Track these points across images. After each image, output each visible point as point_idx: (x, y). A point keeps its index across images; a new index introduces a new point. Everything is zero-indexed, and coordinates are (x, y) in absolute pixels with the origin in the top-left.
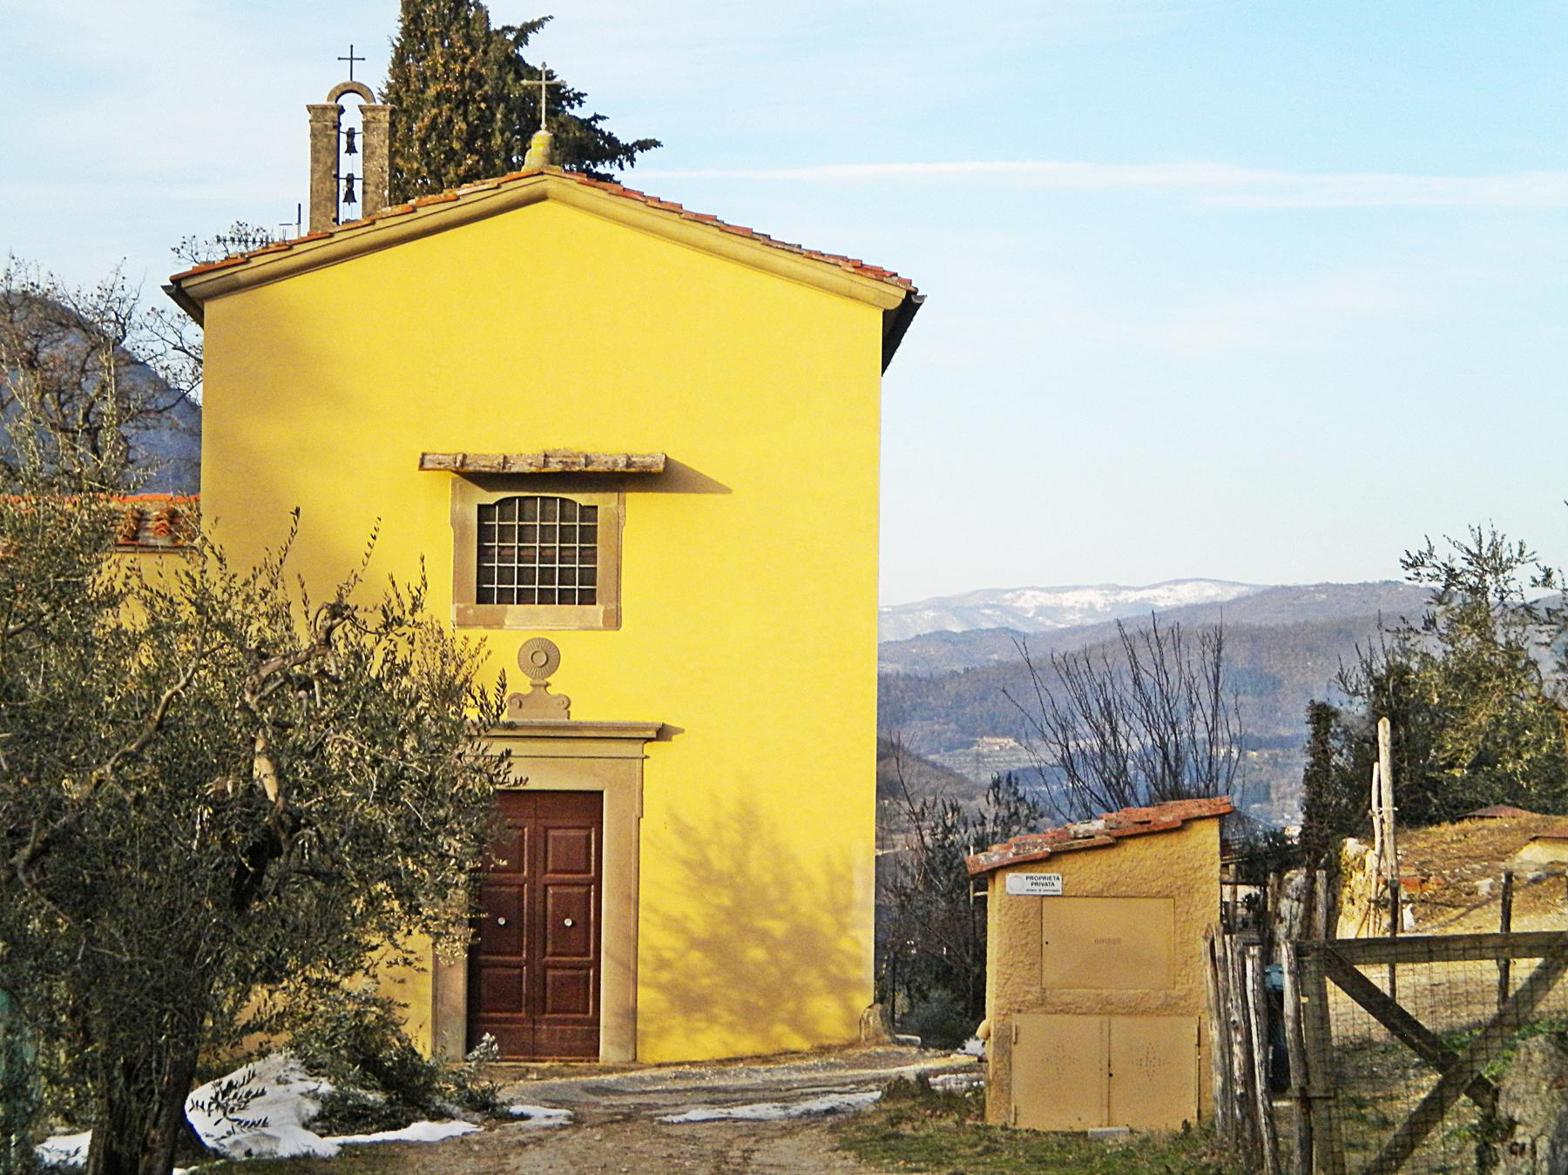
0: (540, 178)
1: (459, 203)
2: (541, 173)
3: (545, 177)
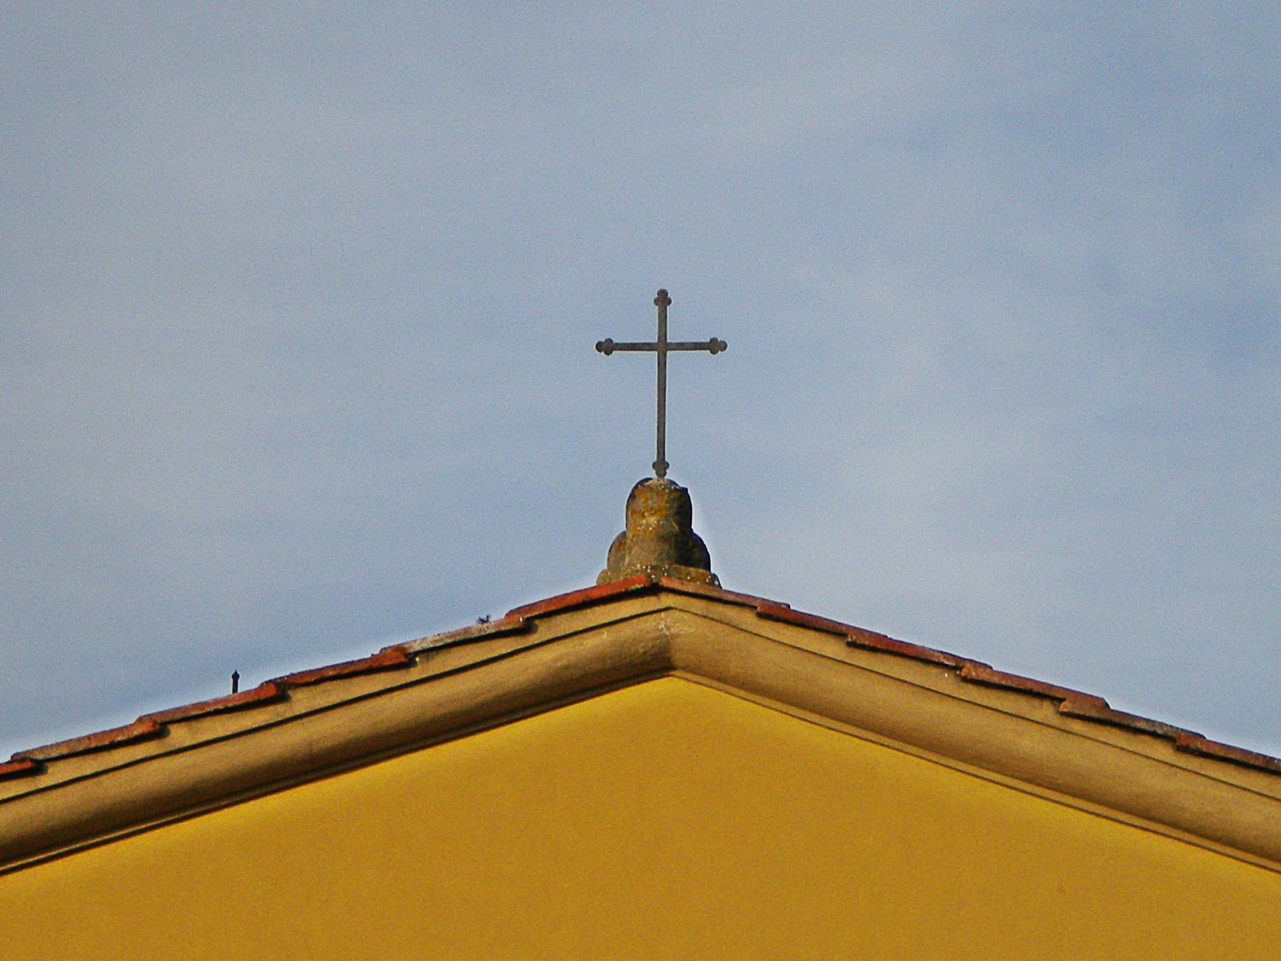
0: (649, 603)
1: (414, 674)
2: (653, 589)
3: (666, 600)
